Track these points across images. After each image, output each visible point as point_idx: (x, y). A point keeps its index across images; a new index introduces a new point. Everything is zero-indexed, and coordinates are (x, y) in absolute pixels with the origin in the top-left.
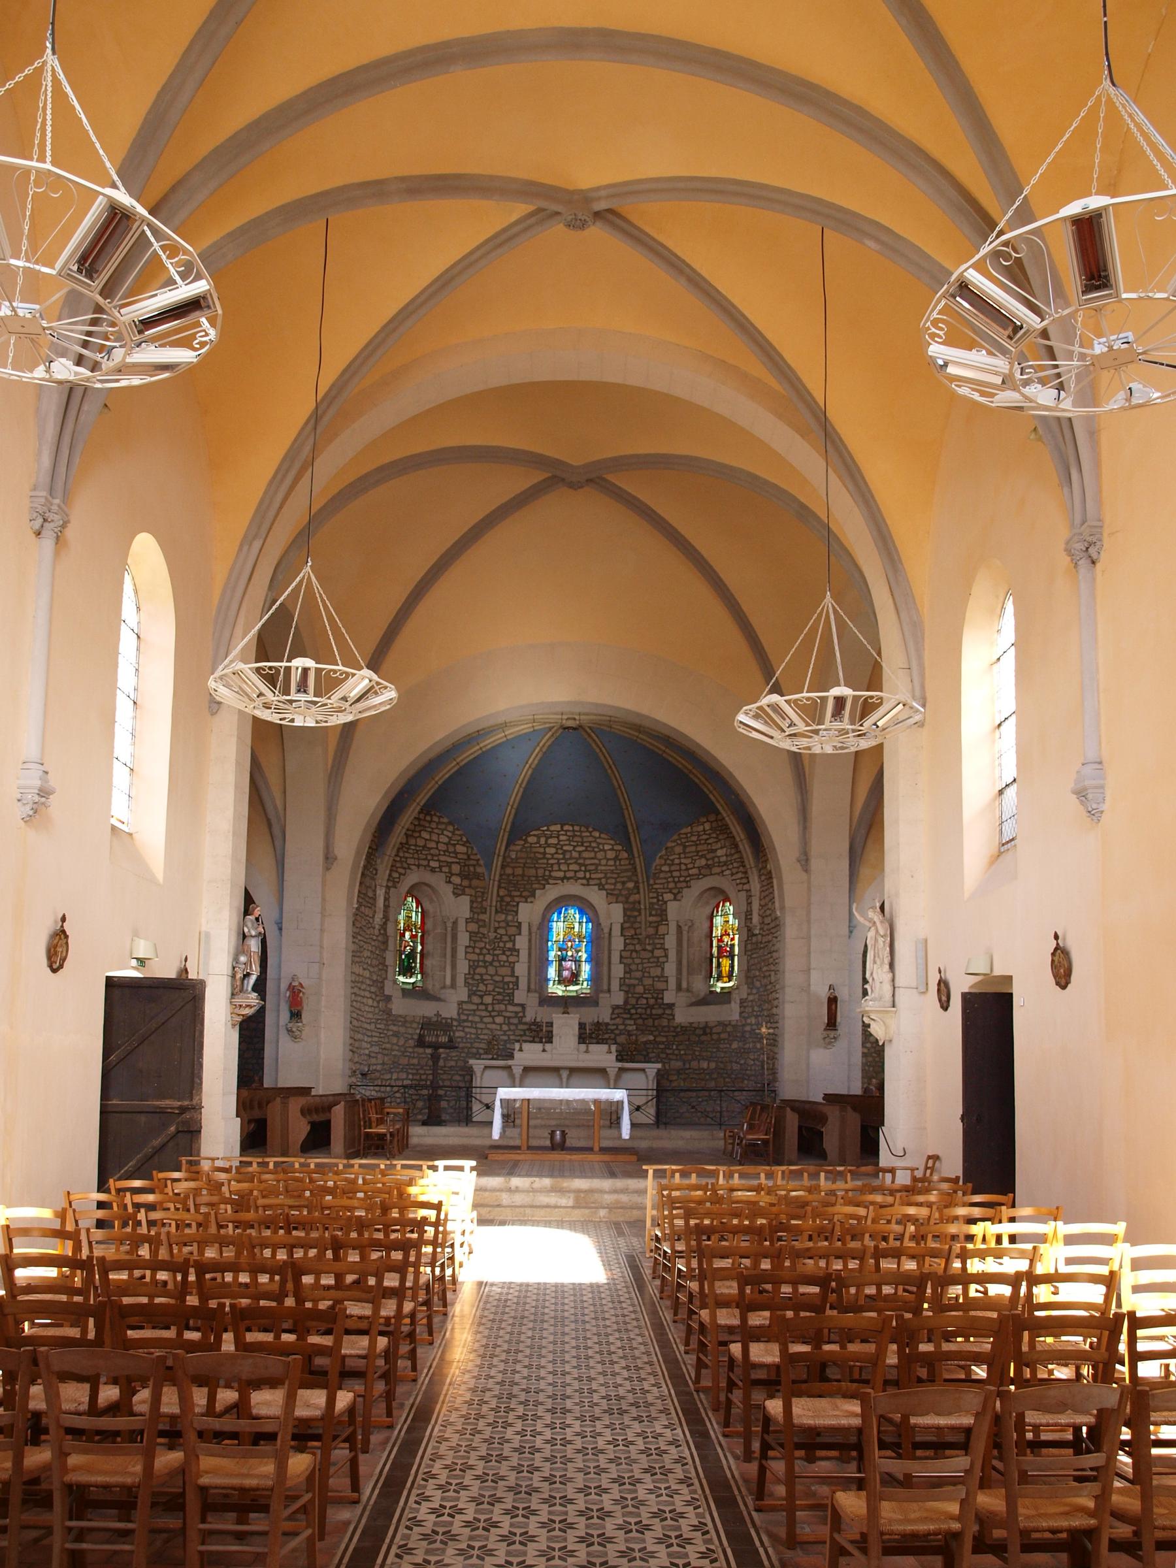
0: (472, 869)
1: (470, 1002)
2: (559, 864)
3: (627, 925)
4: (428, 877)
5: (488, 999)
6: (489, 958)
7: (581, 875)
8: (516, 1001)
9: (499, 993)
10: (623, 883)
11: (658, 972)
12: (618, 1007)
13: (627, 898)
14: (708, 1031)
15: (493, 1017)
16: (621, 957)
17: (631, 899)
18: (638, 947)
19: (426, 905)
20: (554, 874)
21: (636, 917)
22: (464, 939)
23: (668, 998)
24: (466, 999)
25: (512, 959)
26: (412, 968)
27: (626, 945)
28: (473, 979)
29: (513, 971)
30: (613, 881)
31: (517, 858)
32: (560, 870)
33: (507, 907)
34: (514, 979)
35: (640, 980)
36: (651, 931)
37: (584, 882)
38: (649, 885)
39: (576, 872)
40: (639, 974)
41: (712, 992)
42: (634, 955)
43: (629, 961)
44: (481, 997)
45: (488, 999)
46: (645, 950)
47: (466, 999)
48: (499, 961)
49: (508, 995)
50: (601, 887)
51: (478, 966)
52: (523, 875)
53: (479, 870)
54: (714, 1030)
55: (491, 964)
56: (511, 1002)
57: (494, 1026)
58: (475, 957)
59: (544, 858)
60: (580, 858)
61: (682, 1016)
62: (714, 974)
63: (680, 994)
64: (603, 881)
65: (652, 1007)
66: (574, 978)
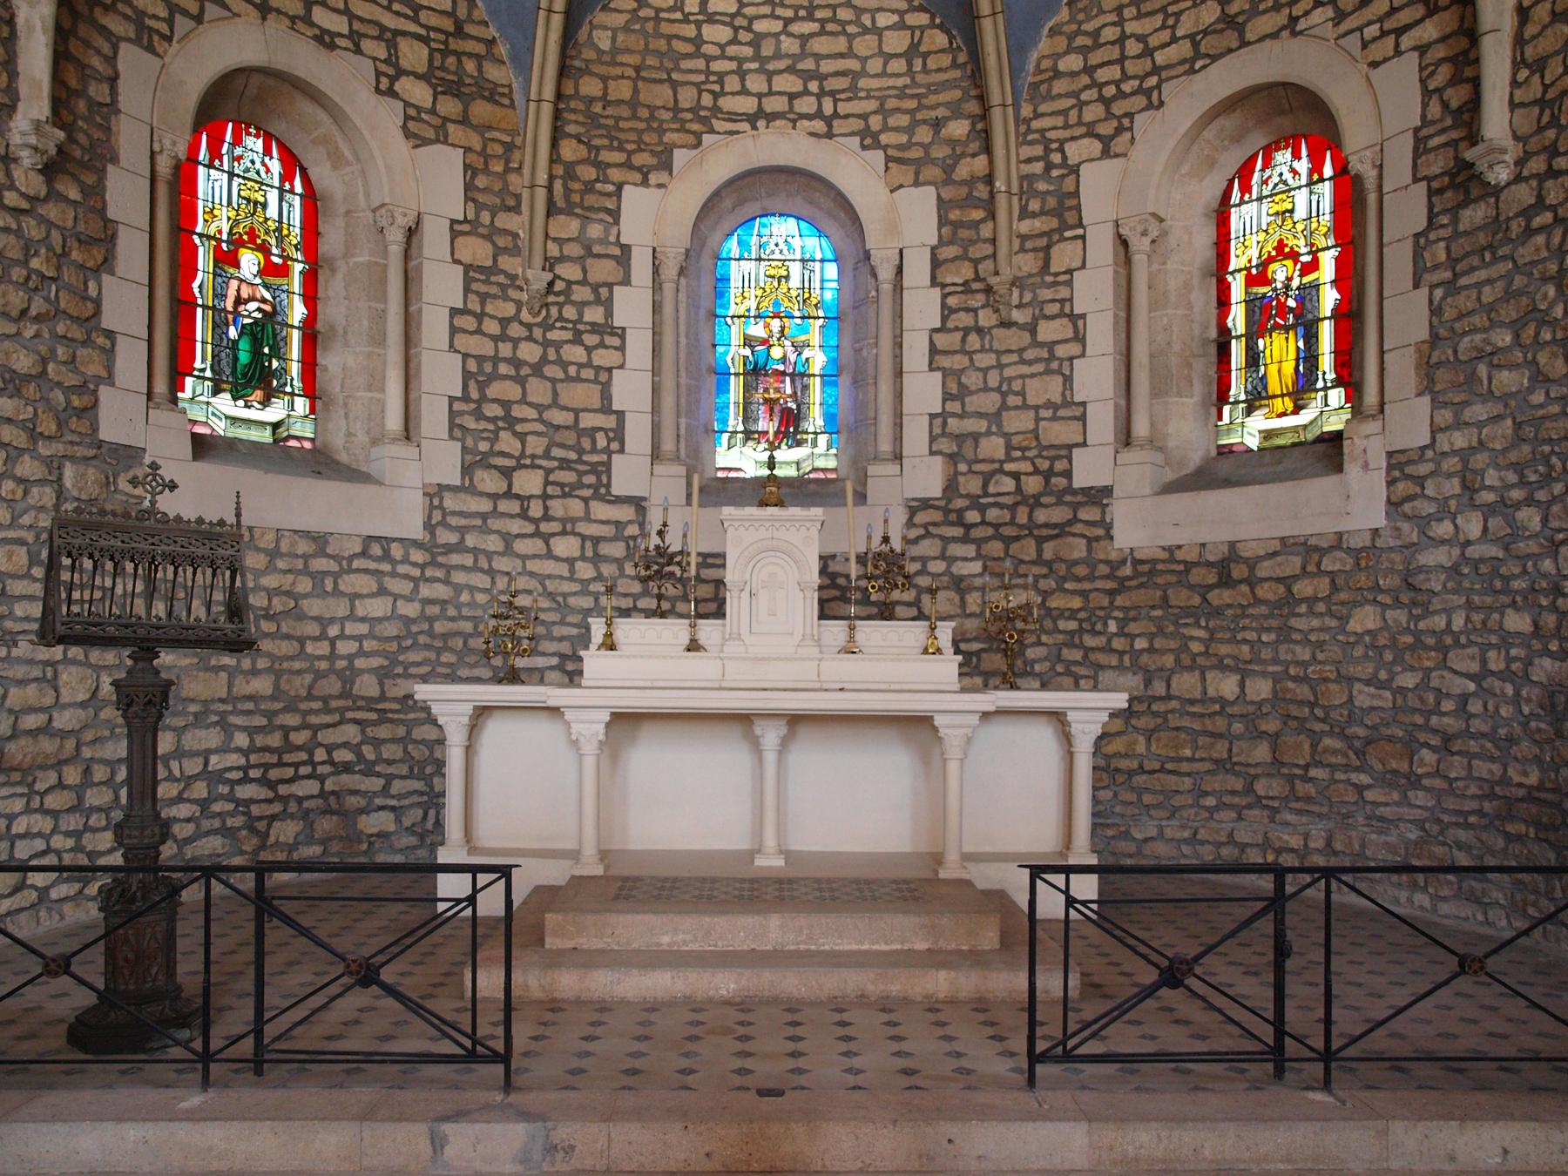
0: (470, 66)
1: (469, 489)
2: (742, 74)
3: (950, 252)
4: (303, 59)
5: (528, 483)
6: (529, 352)
7: (806, 105)
8: (616, 490)
9: (565, 464)
10: (937, 124)
11: (1052, 388)
12: (925, 504)
13: (949, 169)
14: (1238, 572)
15: (546, 538)
16: (934, 351)
17: (962, 172)
18: (986, 318)
19: (322, 175)
20: (726, 103)
21: (975, 225)
22: (443, 286)
23: (1089, 470)
24: (455, 479)
25: (603, 358)
26: (272, 374)
27: (947, 312)
28: (479, 415)
29: (606, 396)
30: (904, 120)
31: (615, 51)
32: (744, 92)
33: (582, 195)
34: (610, 422)
35: (995, 417)
36: (1028, 264)
37: (819, 126)
38: (1018, 120)
39: (792, 97)
40: (990, 402)
41: (1225, 451)
42: (974, 341)
43: (959, 361)
44: (507, 473)
45: (528, 483)
46: (1006, 324)
47: (455, 479)
48: (564, 365)
49: (594, 469)
50: (869, 139)
51: (495, 377)
52: (634, 103)
53: (494, 73)
54: (1265, 569)
55: (537, 369)
56: (601, 492)
57: (549, 567)
58: (486, 347)
59: (697, 54)
60: (803, 55)
61: (1138, 527)
62: (1237, 389)
63: (1127, 456)
64: (875, 122)
65: (1035, 502)
66: (791, 425)
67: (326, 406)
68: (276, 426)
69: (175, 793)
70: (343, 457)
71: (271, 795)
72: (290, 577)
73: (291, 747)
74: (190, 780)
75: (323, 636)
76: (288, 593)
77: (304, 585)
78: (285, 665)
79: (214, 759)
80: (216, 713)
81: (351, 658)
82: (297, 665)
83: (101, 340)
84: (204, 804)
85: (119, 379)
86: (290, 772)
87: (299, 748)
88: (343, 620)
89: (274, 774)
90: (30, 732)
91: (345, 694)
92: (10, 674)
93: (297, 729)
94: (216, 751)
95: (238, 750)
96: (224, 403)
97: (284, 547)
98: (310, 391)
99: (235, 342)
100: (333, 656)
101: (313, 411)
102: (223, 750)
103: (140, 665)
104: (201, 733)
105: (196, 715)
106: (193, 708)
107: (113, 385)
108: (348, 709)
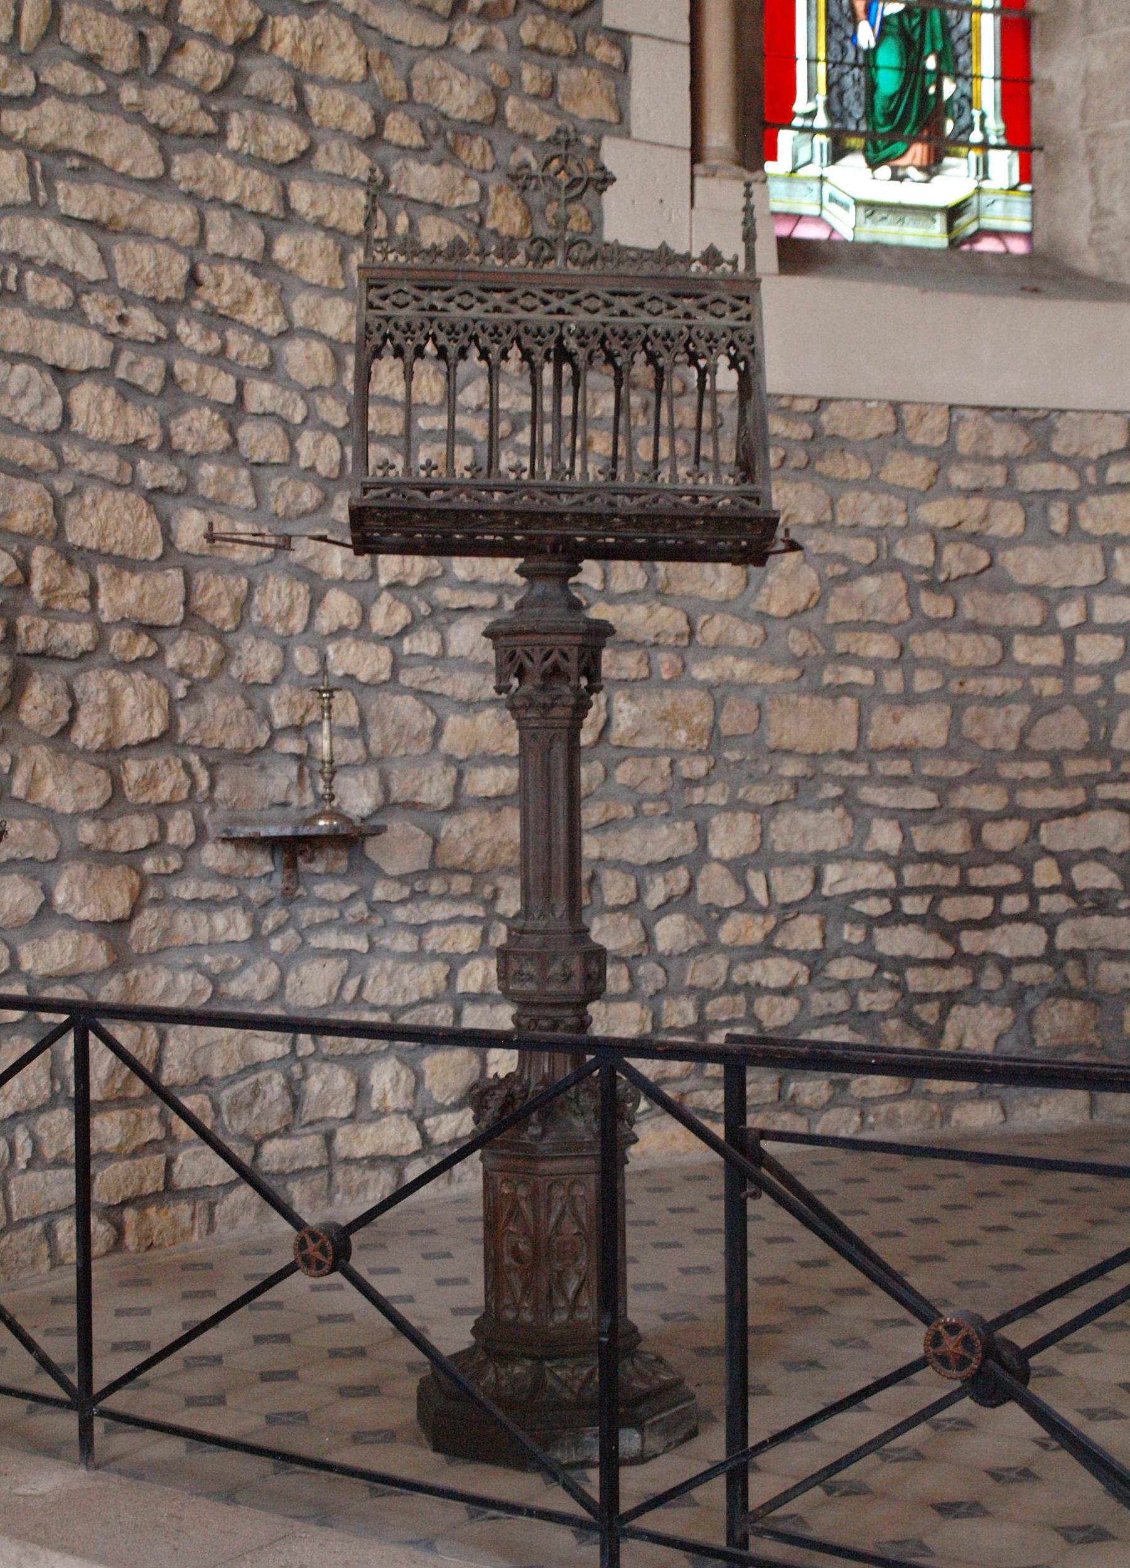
67: (1053, 163)
68: (953, 213)
69: (757, 935)
70: (1090, 263)
71: (946, 951)
72: (978, 505)
73: (981, 854)
74: (788, 912)
75: (1047, 627)
76: (974, 537)
77: (1007, 520)
78: (972, 685)
79: (832, 873)
80: (836, 779)
81: (1107, 671)
82: (996, 685)
83: (604, 52)
84: (815, 961)
85: (639, 124)
86: (983, 906)
87: (1002, 858)
88: (1089, 592)
89: (952, 909)
90: (486, 801)
91: (1097, 747)
92: (447, 688)
93: (997, 818)
94: (837, 857)
95: (880, 856)
96: (854, 175)
97: (965, 441)
98: (1020, 134)
99: (871, 53)
100: (1068, 668)
101: (1026, 175)
102: (849, 855)
103: (540, 588)
104: (807, 820)
105: (796, 782)
106: (791, 768)
107: (627, 135)
108: (1102, 779)
